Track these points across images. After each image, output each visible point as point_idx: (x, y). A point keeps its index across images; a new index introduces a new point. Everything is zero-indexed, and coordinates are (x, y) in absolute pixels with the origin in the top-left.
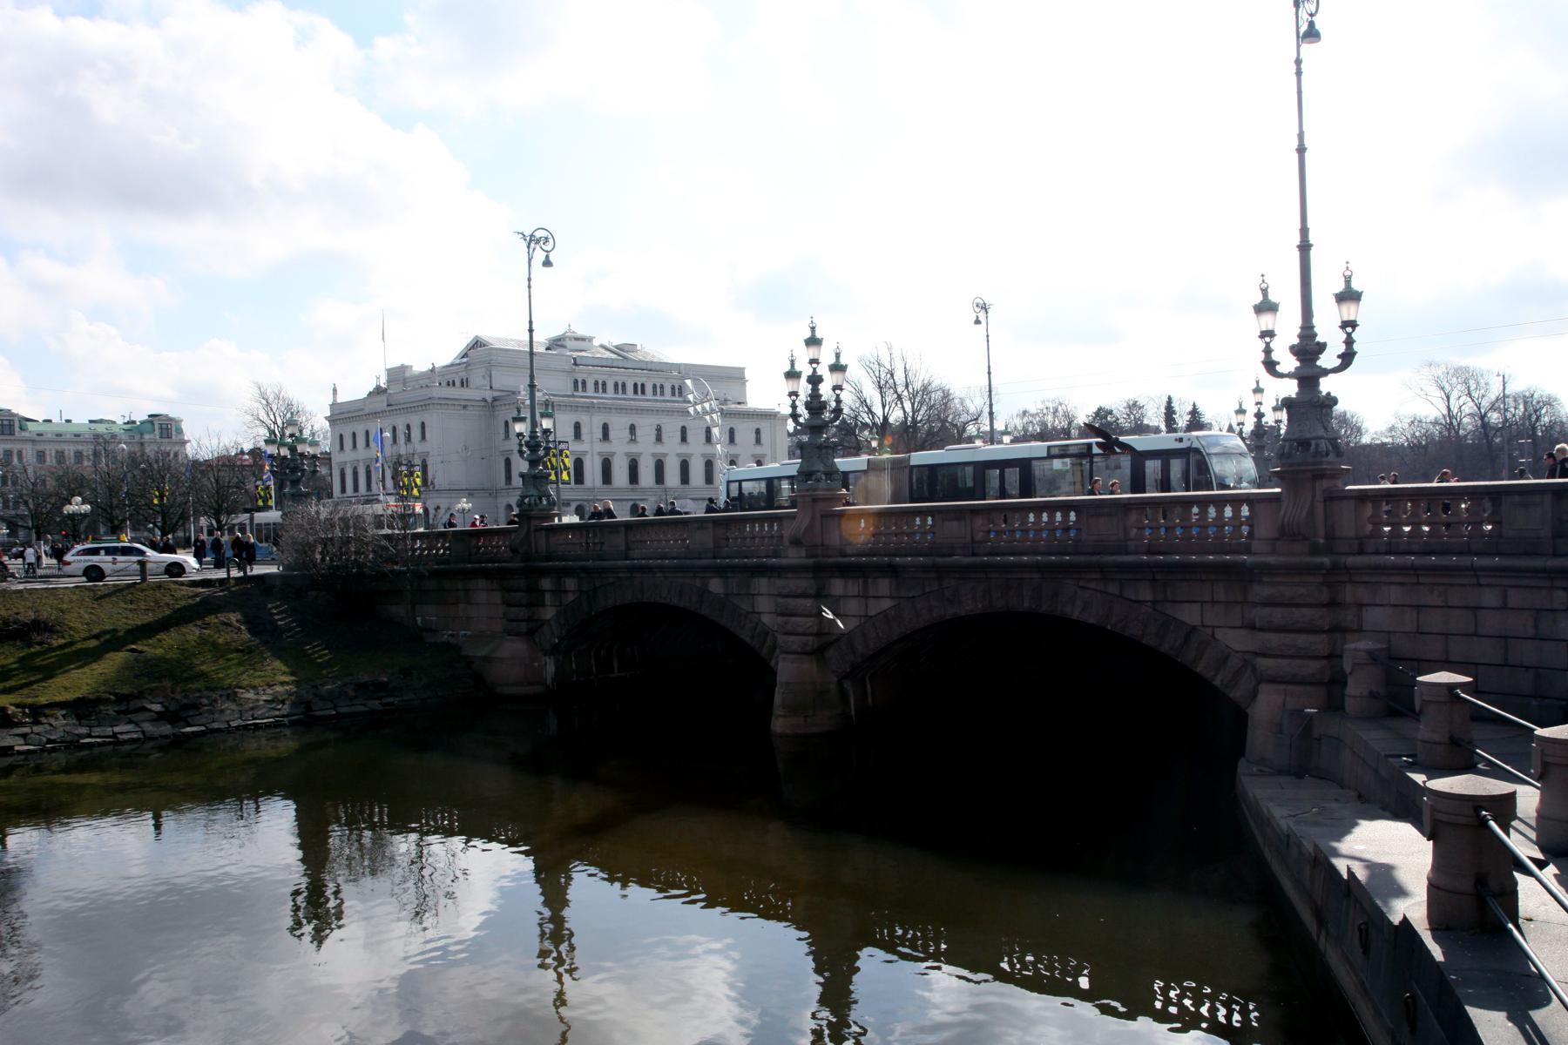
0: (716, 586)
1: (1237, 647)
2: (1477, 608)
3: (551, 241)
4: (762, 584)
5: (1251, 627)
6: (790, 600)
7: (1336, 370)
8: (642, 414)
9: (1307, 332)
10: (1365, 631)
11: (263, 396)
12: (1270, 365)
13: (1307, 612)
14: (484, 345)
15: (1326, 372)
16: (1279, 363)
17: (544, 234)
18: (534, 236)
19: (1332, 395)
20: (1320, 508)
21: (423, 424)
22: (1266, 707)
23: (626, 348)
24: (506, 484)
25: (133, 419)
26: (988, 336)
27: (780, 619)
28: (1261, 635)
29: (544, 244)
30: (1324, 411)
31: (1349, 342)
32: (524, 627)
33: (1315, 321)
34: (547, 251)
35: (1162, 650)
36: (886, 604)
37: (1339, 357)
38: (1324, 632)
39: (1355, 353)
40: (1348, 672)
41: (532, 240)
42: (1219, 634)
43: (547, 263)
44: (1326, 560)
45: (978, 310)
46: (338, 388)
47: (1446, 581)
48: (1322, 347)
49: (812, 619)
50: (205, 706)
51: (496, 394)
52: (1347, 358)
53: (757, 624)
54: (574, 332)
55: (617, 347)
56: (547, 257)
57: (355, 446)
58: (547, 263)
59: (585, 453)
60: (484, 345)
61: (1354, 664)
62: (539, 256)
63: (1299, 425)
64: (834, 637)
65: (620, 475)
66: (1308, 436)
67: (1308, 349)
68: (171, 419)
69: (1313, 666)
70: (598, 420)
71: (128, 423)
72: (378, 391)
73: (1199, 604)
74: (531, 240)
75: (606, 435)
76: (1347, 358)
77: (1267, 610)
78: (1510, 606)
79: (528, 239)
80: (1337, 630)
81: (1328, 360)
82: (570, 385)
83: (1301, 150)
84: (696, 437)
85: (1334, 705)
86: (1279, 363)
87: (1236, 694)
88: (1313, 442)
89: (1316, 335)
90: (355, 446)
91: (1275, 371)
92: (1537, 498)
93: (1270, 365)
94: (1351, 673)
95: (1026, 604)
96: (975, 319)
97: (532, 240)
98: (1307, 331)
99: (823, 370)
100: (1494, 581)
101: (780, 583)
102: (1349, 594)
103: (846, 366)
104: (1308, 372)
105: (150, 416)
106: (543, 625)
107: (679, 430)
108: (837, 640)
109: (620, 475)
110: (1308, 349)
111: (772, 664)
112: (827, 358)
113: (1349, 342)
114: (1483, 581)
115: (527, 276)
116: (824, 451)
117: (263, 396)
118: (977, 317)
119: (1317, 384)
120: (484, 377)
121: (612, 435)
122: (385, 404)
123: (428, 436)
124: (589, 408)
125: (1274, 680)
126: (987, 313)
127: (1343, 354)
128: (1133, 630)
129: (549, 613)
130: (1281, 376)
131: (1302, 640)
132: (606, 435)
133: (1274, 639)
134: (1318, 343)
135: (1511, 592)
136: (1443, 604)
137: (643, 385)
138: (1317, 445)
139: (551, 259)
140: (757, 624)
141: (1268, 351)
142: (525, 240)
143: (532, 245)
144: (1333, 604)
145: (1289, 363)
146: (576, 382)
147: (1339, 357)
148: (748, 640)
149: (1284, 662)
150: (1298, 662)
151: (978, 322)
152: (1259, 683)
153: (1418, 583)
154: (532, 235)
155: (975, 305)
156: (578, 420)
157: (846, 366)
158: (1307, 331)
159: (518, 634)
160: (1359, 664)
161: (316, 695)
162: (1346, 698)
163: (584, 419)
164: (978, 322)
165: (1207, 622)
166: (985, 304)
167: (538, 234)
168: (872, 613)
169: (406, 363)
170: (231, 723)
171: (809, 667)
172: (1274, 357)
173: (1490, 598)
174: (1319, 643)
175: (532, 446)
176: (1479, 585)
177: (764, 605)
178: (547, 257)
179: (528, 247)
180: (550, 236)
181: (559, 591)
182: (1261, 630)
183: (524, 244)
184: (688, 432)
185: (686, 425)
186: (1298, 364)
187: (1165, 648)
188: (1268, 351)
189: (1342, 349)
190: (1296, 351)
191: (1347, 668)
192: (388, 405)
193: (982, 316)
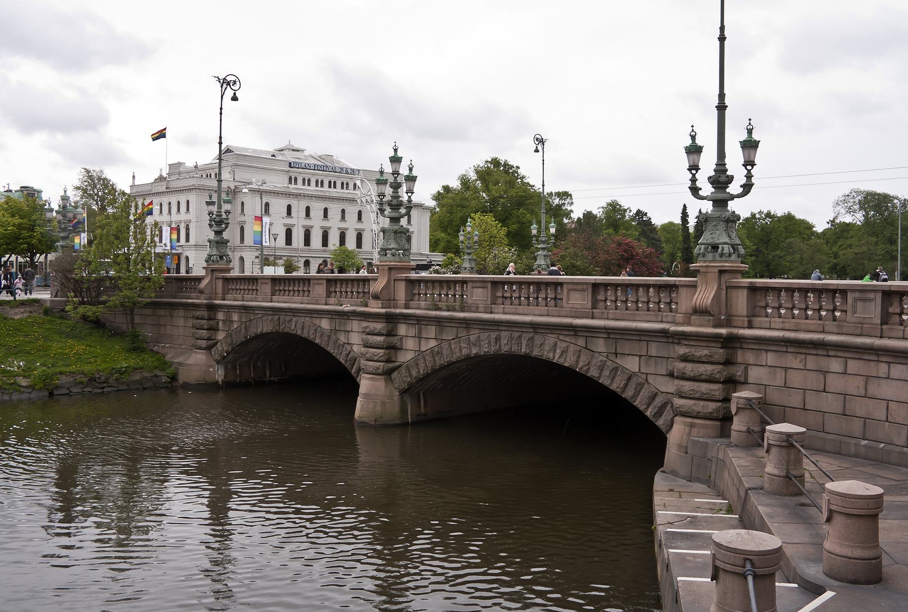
0: (325, 324)
1: (663, 389)
2: (826, 372)
3: (238, 83)
4: (355, 325)
5: (671, 375)
6: (369, 337)
7: (739, 196)
8: (333, 201)
9: (721, 168)
10: (749, 383)
11: (90, 177)
12: (695, 190)
13: (709, 368)
14: (233, 152)
15: (732, 197)
16: (701, 189)
17: (234, 78)
18: (226, 80)
19: (736, 213)
20: (651, 313)
21: (188, 202)
22: (676, 435)
23: (326, 158)
24: (241, 243)
25: (10, 189)
26: (543, 160)
27: (363, 350)
28: (676, 382)
29: (233, 85)
30: (730, 225)
31: (749, 176)
32: (204, 343)
33: (727, 161)
34: (235, 90)
35: (612, 388)
36: (433, 343)
37: (741, 186)
38: (721, 383)
39: (753, 185)
40: (733, 414)
41: (225, 83)
42: (651, 379)
43: (235, 98)
44: (723, 331)
45: (537, 143)
46: (135, 175)
47: (804, 351)
48: (730, 179)
49: (383, 351)
50: (782, 237)
51: (237, 184)
52: (747, 188)
53: (350, 352)
54: (292, 146)
55: (320, 157)
56: (235, 94)
57: (179, 210)
58: (235, 98)
59: (293, 225)
60: (233, 152)
61: (738, 408)
62: (229, 93)
63: (711, 234)
64: (398, 364)
65: (334, 240)
66: (717, 242)
67: (721, 180)
68: (35, 190)
69: (712, 406)
70: (303, 204)
71: (7, 191)
72: (161, 179)
73: (637, 358)
74: (223, 82)
75: (289, 212)
76: (747, 188)
77: (682, 365)
78: (848, 372)
79: (222, 81)
80: (732, 383)
81: (734, 188)
82: (287, 180)
83: (722, 39)
84: (352, 216)
85: (724, 433)
86: (701, 189)
87: (660, 423)
88: (720, 246)
89: (727, 170)
90: (179, 210)
91: (698, 194)
92: (872, 296)
93: (695, 190)
94: (735, 414)
95: (523, 350)
96: (535, 148)
97: (225, 83)
98: (721, 167)
99: (400, 179)
100: (839, 354)
101: (365, 324)
102: (740, 356)
103: (416, 177)
104: (720, 196)
105: (21, 187)
106: (217, 343)
107: (357, 212)
108: (400, 366)
109: (334, 240)
110: (721, 180)
111: (358, 380)
112: (404, 170)
113: (749, 176)
114: (831, 353)
115: (220, 107)
116: (399, 235)
117: (90, 177)
118: (537, 147)
119: (727, 206)
120: (230, 172)
121: (312, 213)
122: (165, 187)
123: (190, 209)
124: (297, 196)
125: (684, 415)
126: (544, 145)
127: (744, 185)
128: (593, 373)
129: (221, 336)
130: (702, 198)
131: (704, 387)
132: (289, 212)
133: (687, 386)
134: (728, 176)
135: (850, 362)
136: (804, 368)
137: (335, 182)
138: (723, 249)
139: (237, 95)
140: (350, 352)
141: (694, 180)
142: (220, 82)
143: (225, 86)
144: (728, 362)
145: (707, 189)
146: (290, 178)
147: (741, 186)
148: (343, 362)
149: (691, 402)
150: (702, 403)
151: (537, 151)
152: (676, 416)
153: (787, 352)
154: (225, 79)
155: (535, 139)
156: (290, 203)
157: (416, 177)
158: (721, 167)
159: (200, 348)
160: (742, 408)
161: (887, 223)
162: (732, 431)
163: (294, 203)
164: (537, 151)
165: (643, 370)
166: (542, 139)
167: (229, 79)
168: (423, 349)
169: (181, 161)
170: (71, 389)
171: (380, 384)
172: (698, 184)
173: (835, 365)
174: (716, 389)
175: (217, 222)
176: (828, 356)
177: (356, 339)
178: (235, 94)
179: (222, 87)
180: (237, 80)
181: (228, 321)
182: (677, 378)
183: (219, 85)
184: (363, 214)
185: (362, 210)
186: (713, 190)
187: (613, 387)
188: (694, 180)
189: (744, 181)
190: (713, 181)
191: (734, 411)
192: (166, 188)
193: (540, 148)
